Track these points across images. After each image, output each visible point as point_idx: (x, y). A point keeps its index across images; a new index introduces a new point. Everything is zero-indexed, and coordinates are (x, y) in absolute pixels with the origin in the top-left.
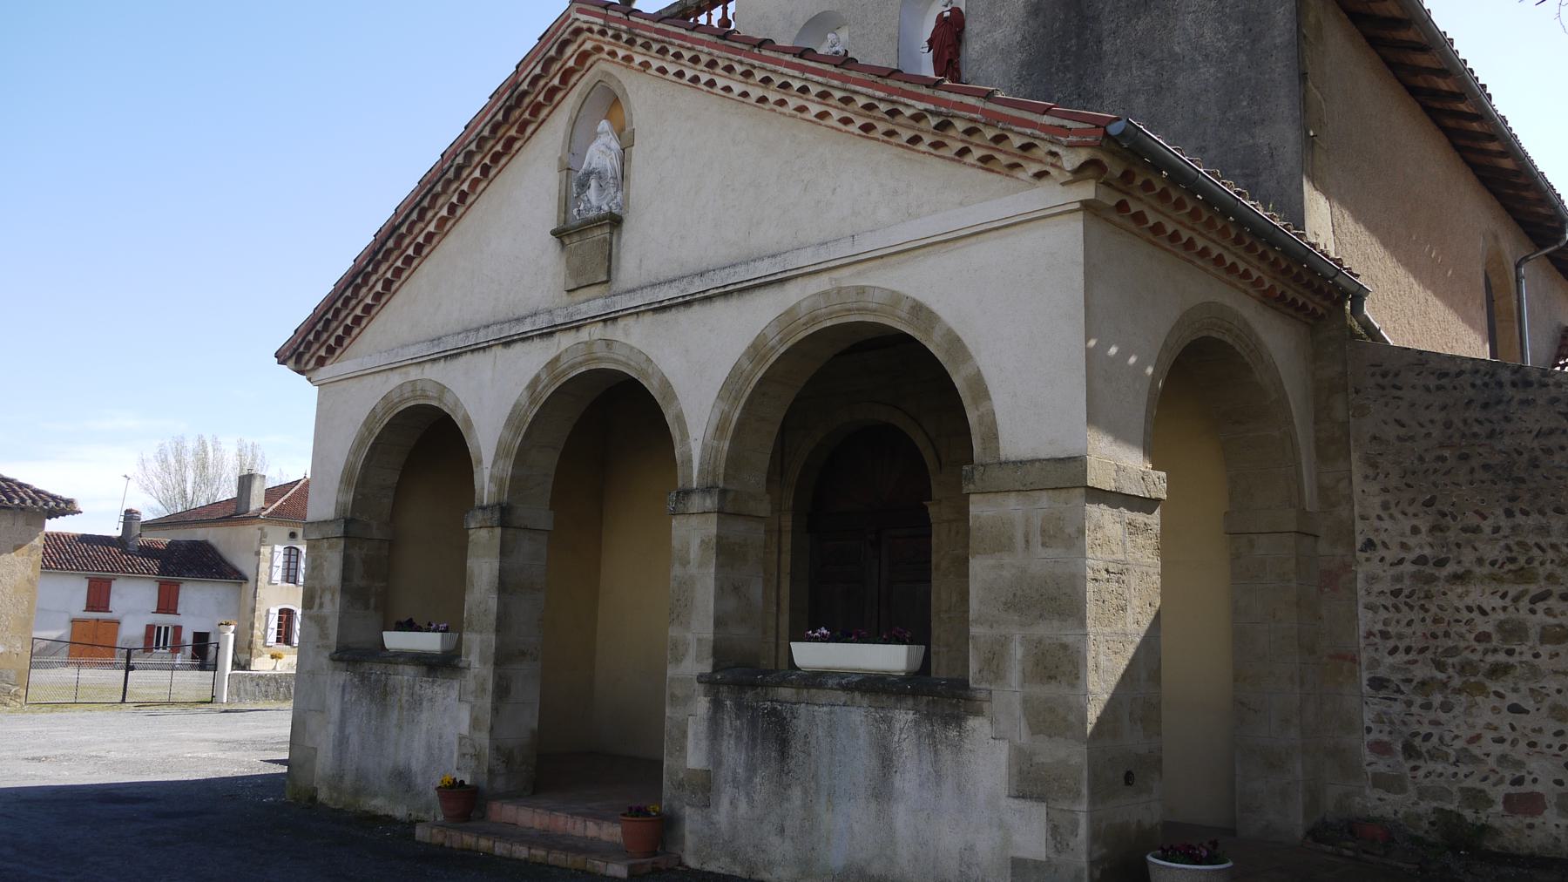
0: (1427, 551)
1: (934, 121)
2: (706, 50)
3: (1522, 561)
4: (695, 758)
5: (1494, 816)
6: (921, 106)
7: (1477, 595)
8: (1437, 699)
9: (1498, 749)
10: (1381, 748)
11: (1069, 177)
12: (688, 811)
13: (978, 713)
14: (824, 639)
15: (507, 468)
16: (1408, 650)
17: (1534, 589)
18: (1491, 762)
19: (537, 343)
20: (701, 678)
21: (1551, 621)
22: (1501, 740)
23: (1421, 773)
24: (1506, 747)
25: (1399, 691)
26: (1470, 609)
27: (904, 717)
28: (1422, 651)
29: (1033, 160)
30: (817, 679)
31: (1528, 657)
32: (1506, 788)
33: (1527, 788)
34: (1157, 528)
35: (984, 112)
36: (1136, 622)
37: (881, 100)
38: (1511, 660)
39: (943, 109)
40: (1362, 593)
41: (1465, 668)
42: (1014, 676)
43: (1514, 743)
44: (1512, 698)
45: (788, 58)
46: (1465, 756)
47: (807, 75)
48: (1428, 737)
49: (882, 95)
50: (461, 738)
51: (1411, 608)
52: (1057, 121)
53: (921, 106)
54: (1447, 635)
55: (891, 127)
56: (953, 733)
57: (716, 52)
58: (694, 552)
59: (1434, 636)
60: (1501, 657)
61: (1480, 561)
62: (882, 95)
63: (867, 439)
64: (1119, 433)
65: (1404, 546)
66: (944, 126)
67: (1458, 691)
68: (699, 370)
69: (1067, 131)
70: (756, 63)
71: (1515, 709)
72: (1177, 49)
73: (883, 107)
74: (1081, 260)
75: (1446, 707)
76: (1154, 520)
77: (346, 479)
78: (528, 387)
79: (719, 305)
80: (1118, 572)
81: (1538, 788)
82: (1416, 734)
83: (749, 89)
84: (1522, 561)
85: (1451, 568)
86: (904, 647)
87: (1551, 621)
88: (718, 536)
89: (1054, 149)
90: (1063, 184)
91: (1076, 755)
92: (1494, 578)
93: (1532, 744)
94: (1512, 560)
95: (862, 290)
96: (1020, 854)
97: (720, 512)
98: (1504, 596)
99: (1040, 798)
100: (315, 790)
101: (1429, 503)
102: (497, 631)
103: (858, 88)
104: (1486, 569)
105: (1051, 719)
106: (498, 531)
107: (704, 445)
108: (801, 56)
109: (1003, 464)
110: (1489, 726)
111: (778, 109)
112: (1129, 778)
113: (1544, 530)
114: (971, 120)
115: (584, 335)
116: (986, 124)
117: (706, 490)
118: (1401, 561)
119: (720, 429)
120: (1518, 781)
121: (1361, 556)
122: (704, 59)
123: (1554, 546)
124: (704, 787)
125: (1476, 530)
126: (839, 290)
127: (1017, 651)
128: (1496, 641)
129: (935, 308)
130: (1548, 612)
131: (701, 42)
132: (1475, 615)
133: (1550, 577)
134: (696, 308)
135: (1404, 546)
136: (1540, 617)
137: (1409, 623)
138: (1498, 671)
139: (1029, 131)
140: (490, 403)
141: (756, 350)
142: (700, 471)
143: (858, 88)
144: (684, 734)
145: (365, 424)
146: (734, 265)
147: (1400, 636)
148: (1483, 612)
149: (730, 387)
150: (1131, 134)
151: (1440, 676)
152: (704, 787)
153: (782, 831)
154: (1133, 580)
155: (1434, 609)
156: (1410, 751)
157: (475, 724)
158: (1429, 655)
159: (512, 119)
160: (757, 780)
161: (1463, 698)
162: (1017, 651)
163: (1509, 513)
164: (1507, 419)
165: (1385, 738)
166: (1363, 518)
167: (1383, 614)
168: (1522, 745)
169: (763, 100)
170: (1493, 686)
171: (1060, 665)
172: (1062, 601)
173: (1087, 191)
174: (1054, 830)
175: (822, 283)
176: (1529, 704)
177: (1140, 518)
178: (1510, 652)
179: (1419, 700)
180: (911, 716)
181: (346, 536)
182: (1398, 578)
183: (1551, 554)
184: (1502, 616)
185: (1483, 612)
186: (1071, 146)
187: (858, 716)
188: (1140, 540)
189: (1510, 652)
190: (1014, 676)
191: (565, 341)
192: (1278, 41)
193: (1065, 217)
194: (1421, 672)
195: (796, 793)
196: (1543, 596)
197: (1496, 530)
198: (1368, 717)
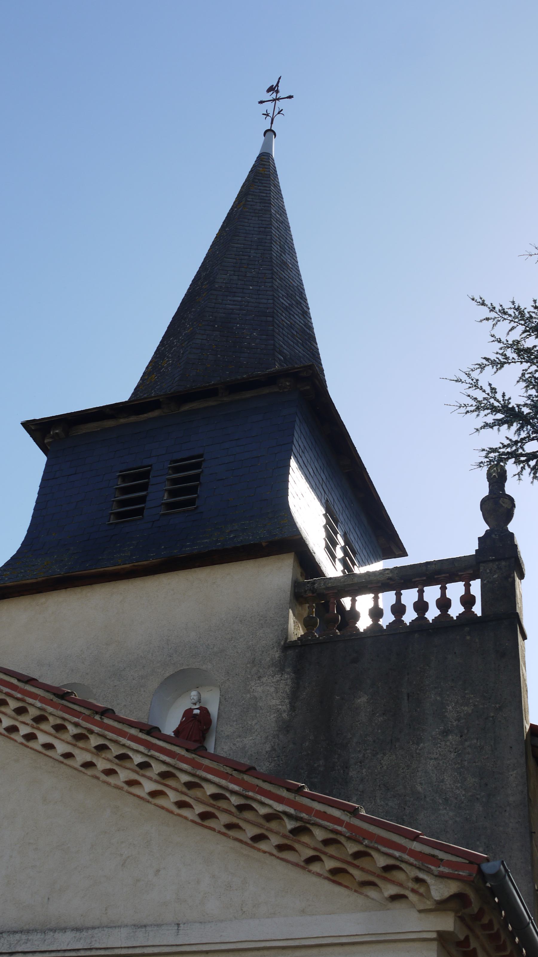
1: (290, 825)
2: (39, 704)
6: (280, 807)
11: (429, 905)
29: (393, 882)
35: (349, 826)
37: (233, 792)
39: (304, 815)
45: (133, 731)
47: (153, 753)
49: (236, 788)
52: (427, 850)
53: (280, 807)
55: (235, 820)
57: (50, 709)
62: (236, 788)
66: (301, 830)
69: (439, 862)
70: (96, 729)
72: (419, 788)
73: (235, 800)
83: (76, 752)
89: (422, 875)
90: (420, 911)
103: (210, 777)
108: (148, 733)
111: (103, 777)
114: (333, 831)
116: (349, 838)
122: (33, 712)
131: (34, 696)
139: (397, 854)
143: (210, 777)
146: (28, 932)
150: (499, 878)
169: (88, 765)
173: (447, 923)
186: (441, 876)
192: (511, 799)
193: (417, 945)
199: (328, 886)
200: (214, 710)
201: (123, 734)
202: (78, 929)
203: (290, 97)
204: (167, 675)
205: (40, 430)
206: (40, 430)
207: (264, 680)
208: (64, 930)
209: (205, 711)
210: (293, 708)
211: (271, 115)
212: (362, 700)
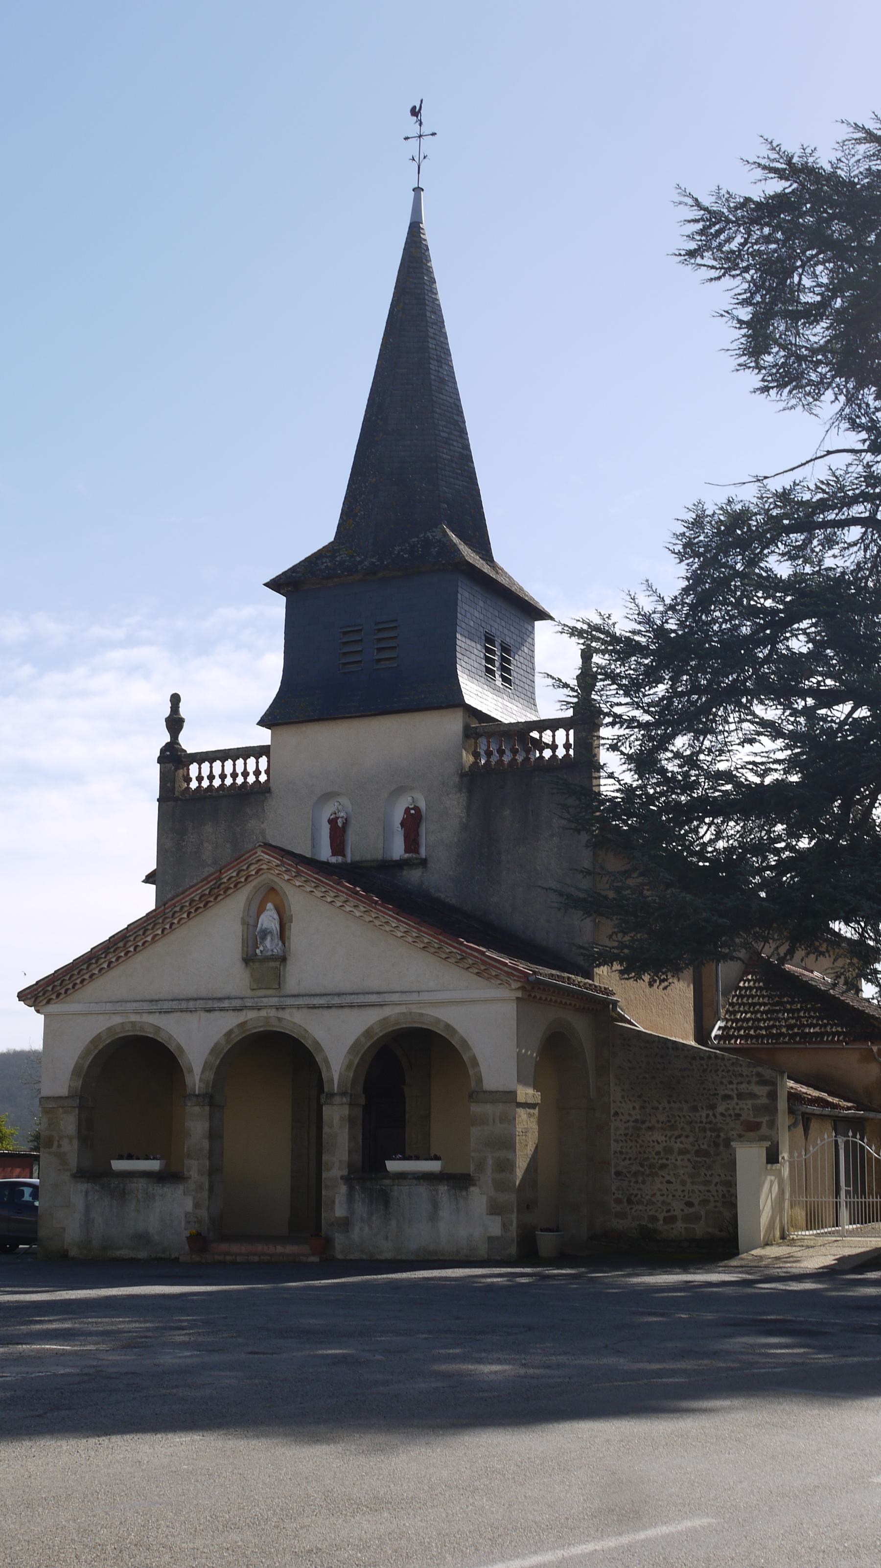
0: (639, 1117)
3: (673, 1122)
4: (340, 1211)
5: (660, 1225)
6: (455, 950)
7: (657, 1136)
8: (640, 1179)
9: (661, 1199)
10: (618, 1201)
12: (336, 1235)
13: (474, 1185)
14: (400, 1159)
15: (210, 1075)
16: (630, 1159)
17: (676, 1133)
18: (659, 1204)
19: (231, 1013)
20: (342, 1178)
21: (682, 1146)
22: (663, 1195)
23: (633, 1210)
24: (664, 1198)
25: (626, 1176)
26: (653, 1141)
27: (443, 1189)
28: (635, 1159)
30: (401, 1176)
31: (673, 1161)
32: (664, 1214)
33: (672, 1213)
34: (537, 1114)
35: (481, 960)
36: (530, 1150)
38: (668, 1162)
40: (612, 1134)
41: (652, 1166)
42: (489, 1170)
43: (668, 1196)
44: (667, 1178)
46: (650, 1202)
48: (636, 1195)
50: (187, 1215)
51: (631, 1141)
52: (510, 970)
54: (645, 1152)
56: (464, 1193)
58: (336, 1121)
59: (640, 1153)
60: (664, 1161)
61: (658, 1122)
63: (409, 1066)
64: (526, 1084)
65: (630, 1114)
67: (648, 1176)
68: (337, 1039)
69: (515, 975)
71: (668, 1182)
72: (538, 867)
74: (515, 1017)
75: (644, 1182)
76: (536, 1111)
77: (76, 1072)
78: (225, 1035)
79: (347, 1011)
80: (525, 1132)
81: (675, 1213)
82: (632, 1194)
84: (673, 1122)
85: (647, 1124)
86: (158, 1161)
87: (682, 1146)
88: (349, 1115)
91: (511, 1198)
92: (663, 1129)
93: (674, 1196)
94: (669, 1121)
95: (421, 1015)
96: (492, 1235)
97: (351, 1105)
98: (666, 1136)
99: (499, 1214)
100: (67, 1251)
101: (640, 1097)
102: (209, 1158)
104: (660, 1125)
105: (501, 1186)
106: (207, 1108)
107: (340, 1074)
109: (485, 1092)
110: (660, 1190)
112: (528, 1207)
113: (681, 1109)
115: (263, 1013)
117: (343, 1094)
118: (628, 1121)
119: (349, 1067)
120: (668, 1211)
121: (613, 1118)
123: (684, 1116)
124: (345, 1224)
125: (657, 1108)
126: (411, 1013)
127: (490, 1162)
128: (662, 1155)
129: (455, 1027)
130: (681, 1143)
132: (656, 1144)
133: (682, 1129)
134: (334, 1010)
135: (630, 1114)
136: (679, 1145)
137: (631, 1148)
138: (663, 1167)
140: (197, 1041)
141: (368, 1033)
142: (338, 1086)
144: (334, 1202)
145: (91, 1042)
146: (357, 994)
147: (627, 1153)
148: (658, 1143)
149: (353, 1048)
151: (641, 1169)
152: (345, 1224)
153: (387, 1238)
154: (530, 1135)
155: (640, 1141)
156: (630, 1202)
157: (197, 1205)
158: (638, 1161)
159: (212, 893)
160: (374, 1218)
161: (650, 1178)
162: (490, 1162)
163: (669, 1102)
164: (670, 1063)
165: (620, 1196)
166: (614, 1102)
167: (621, 1144)
168: (670, 1197)
170: (661, 1173)
171: (506, 1166)
172: (508, 1144)
173: (519, 994)
174: (504, 1225)
175: (403, 1009)
176: (673, 1180)
177: (532, 1111)
178: (667, 1159)
179: (633, 1180)
180: (446, 1188)
181: (80, 1107)
182: (627, 1128)
183: (683, 1119)
184: (665, 1144)
185: (658, 1143)
187: (423, 1190)
188: (532, 1120)
189: (667, 1159)
190: (489, 1170)
191: (251, 1015)
194: (634, 1168)
195: (393, 1223)
196: (679, 1136)
197: (664, 1108)
198: (613, 1189)
199: (476, 977)
200: (422, 805)
201: (387, 914)
202: (379, 993)
203: (434, 134)
204: (392, 789)
205: (275, 585)
206: (275, 585)
207: (451, 796)
208: (372, 993)
209: (417, 808)
210: (468, 815)
211: (417, 159)
212: (507, 813)
